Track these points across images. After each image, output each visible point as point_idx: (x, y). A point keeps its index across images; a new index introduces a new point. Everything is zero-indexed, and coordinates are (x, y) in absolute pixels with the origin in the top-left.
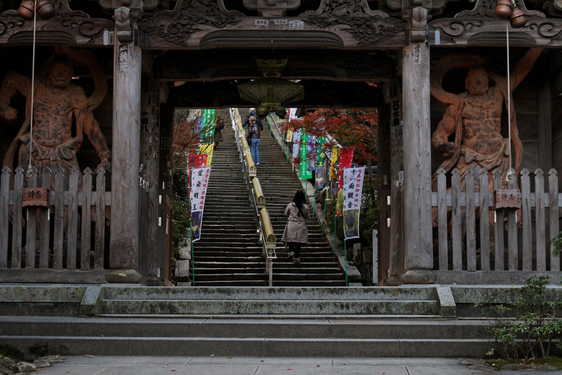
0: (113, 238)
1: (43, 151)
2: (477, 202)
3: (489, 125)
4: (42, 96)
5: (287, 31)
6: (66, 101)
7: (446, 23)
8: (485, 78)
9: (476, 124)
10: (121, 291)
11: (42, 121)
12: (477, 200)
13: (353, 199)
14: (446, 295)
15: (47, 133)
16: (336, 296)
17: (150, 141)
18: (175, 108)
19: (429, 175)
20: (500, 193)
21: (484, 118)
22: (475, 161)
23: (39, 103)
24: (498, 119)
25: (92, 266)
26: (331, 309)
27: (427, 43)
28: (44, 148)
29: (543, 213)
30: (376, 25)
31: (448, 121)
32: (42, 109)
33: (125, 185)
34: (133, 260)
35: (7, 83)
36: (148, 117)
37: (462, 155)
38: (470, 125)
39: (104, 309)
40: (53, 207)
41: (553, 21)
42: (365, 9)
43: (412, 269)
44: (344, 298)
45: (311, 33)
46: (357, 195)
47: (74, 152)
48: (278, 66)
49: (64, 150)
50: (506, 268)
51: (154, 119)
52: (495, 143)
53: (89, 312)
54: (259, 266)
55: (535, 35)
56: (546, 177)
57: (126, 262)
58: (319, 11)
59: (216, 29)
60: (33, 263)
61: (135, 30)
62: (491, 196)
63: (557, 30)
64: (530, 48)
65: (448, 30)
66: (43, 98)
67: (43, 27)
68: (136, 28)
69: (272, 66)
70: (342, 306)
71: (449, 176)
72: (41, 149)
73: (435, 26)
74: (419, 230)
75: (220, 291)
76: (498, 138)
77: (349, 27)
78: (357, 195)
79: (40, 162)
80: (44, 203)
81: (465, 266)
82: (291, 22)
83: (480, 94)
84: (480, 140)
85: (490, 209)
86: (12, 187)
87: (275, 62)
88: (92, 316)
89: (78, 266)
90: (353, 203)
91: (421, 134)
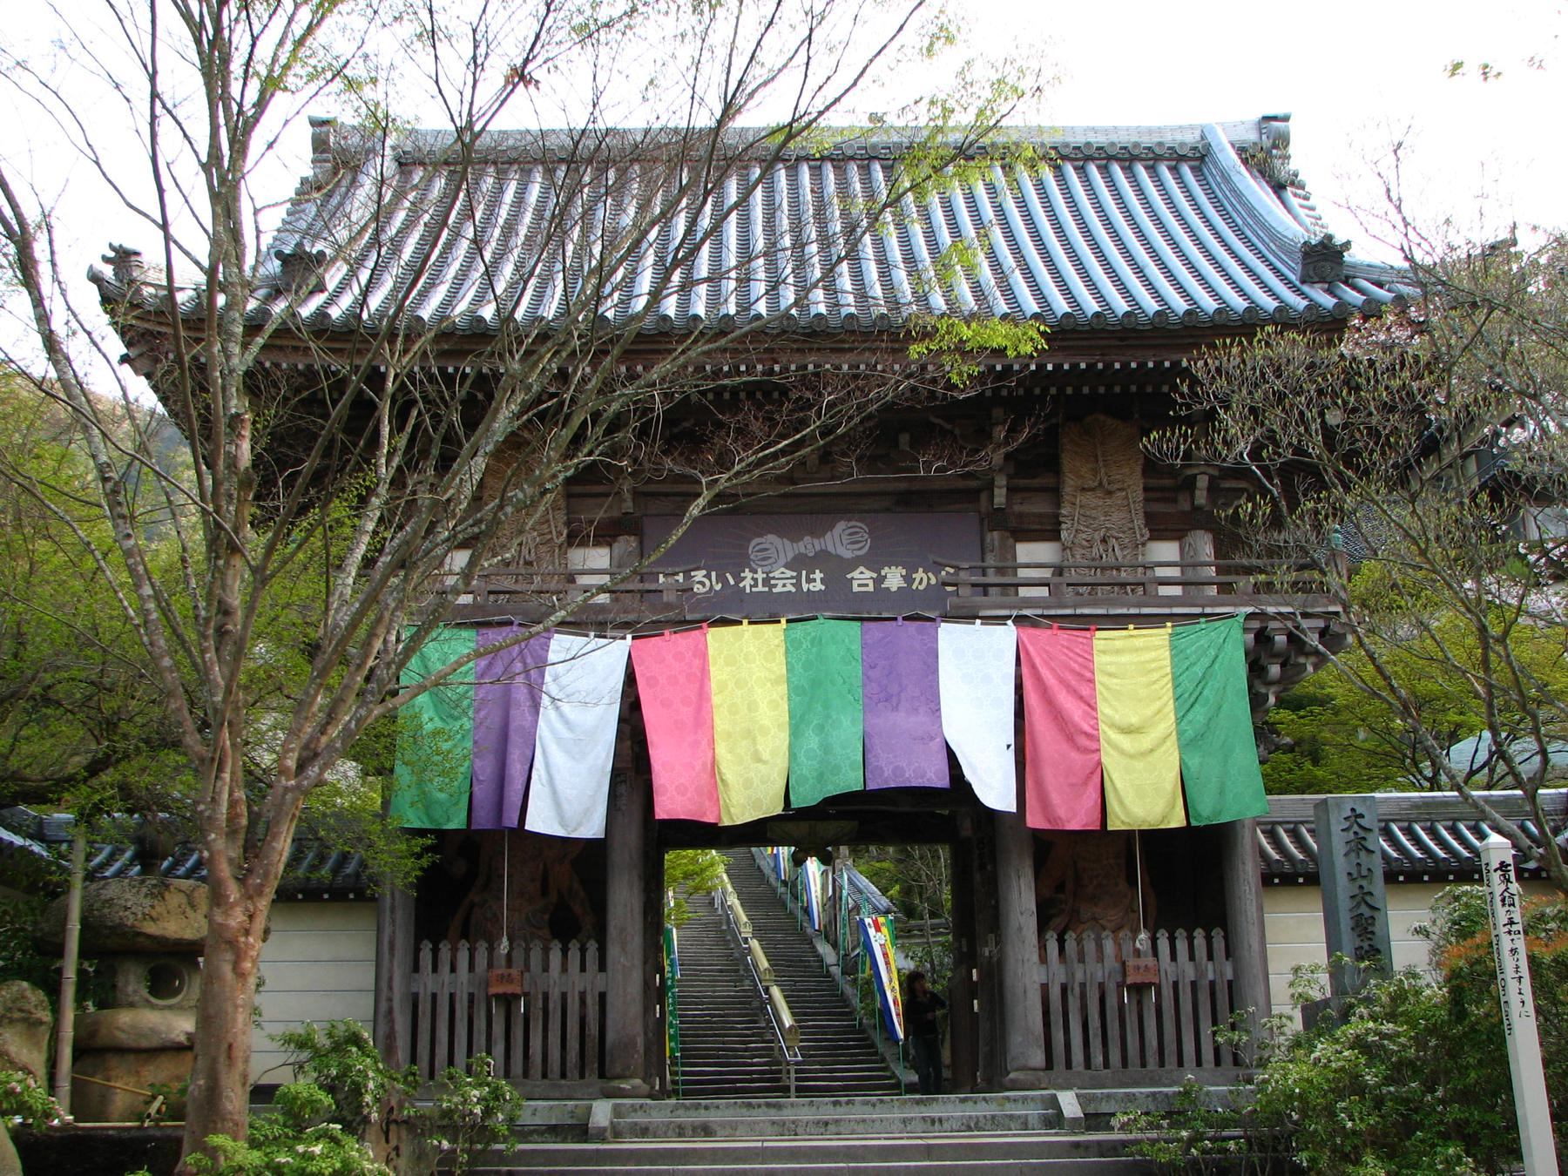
0: (611, 1036)
2: (1099, 977)
10: (634, 1109)
12: (1100, 974)
14: (1069, 1103)
16: (923, 1108)
20: (1131, 962)
25: (582, 1076)
26: (919, 1126)
29: (1188, 989)
39: (617, 1134)
44: (934, 1111)
47: (546, 917)
50: (1144, 1065)
53: (601, 1136)
54: (771, 1072)
56: (1191, 939)
62: (1117, 965)
70: (933, 1121)
74: (1026, 1014)
75: (768, 1105)
80: (518, 990)
81: (1088, 1063)
86: (471, 968)
88: (604, 1140)
89: (563, 1075)
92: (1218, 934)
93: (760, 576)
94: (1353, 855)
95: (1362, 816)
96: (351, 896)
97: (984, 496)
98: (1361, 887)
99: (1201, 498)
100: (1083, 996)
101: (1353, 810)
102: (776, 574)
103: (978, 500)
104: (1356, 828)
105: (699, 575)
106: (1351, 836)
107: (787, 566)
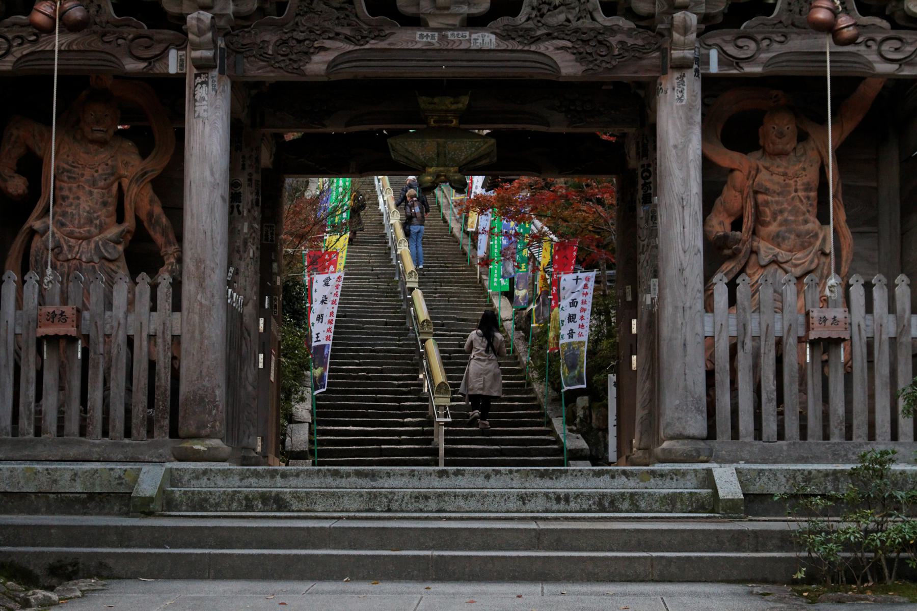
0: (184, 388)
1: (70, 246)
2: (778, 329)
3: (798, 204)
4: (68, 156)
5: (468, 51)
6: (107, 165)
7: (728, 38)
8: (792, 127)
9: (777, 203)
10: (197, 475)
11: (68, 198)
12: (778, 326)
13: (577, 325)
14: (727, 481)
15: (77, 217)
16: (549, 483)
17: (246, 230)
18: (286, 176)
19: (700, 286)
20: (815, 314)
21: (789, 193)
22: (775, 262)
23: (64, 168)
24: (813, 194)
25: (150, 433)
26: (540, 503)
27: (697, 71)
28: (72, 241)
29: (886, 348)
30: (613, 40)
31: (730, 197)
32: (69, 178)
33: (203, 301)
34: (218, 423)
35: (12, 135)
36: (241, 190)
37: (754, 252)
38: (767, 203)
39: (169, 504)
40: (86, 338)
41: (902, 34)
42: (596, 15)
43: (672, 438)
44: (561, 486)
45: (507, 54)
46: (582, 318)
47: (120, 248)
48: (454, 107)
49: (105, 244)
50: (826, 437)
51: (252, 193)
52: (808, 233)
53: (145, 508)
54: (423, 433)
55: (873, 57)
56: (891, 288)
57: (205, 426)
58: (521, 18)
59: (352, 47)
60: (54, 429)
61: (221, 49)
62: (801, 319)
63: (909, 49)
64: (864, 78)
65: (731, 50)
66: (71, 159)
67: (70, 44)
68: (223, 46)
69: (444, 107)
70: (558, 499)
71: (732, 286)
72: (67, 242)
73: (710, 42)
74: (684, 375)
75: (359, 474)
76: (813, 224)
77: (569, 44)
78: (582, 318)
79: (65, 264)
80: (72, 331)
81: (758, 433)
82: (474, 36)
83: (783, 154)
84: (783, 228)
85: (800, 340)
86: (19, 305)
87: (448, 100)
88: (150, 514)
89: (128, 434)
90: (577, 330)
91: (687, 218)
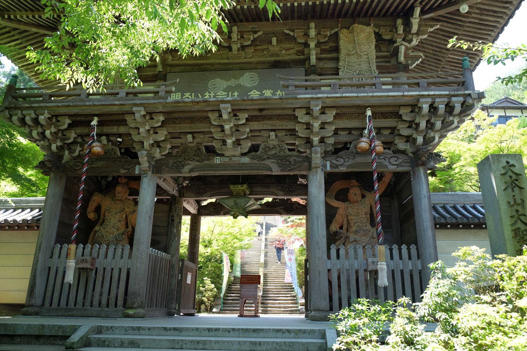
2: (356, 266)
3: (363, 220)
5: (239, 164)
7: (333, 158)
8: (359, 192)
9: (355, 219)
12: (356, 265)
19: (325, 249)
21: (359, 215)
22: (355, 241)
24: (368, 216)
27: (322, 169)
28: (108, 234)
30: (291, 159)
31: (339, 218)
37: (347, 237)
38: (351, 219)
41: (397, 155)
42: (285, 151)
43: (315, 310)
45: (253, 165)
48: (241, 188)
49: (119, 235)
52: (367, 230)
55: (387, 163)
56: (400, 250)
57: (135, 304)
58: (259, 152)
59: (198, 163)
60: (81, 304)
63: (400, 160)
65: (334, 162)
73: (327, 159)
76: (369, 227)
77: (276, 161)
80: (88, 266)
82: (241, 159)
83: (356, 202)
84: (358, 228)
85: (366, 271)
87: (240, 186)
91: (319, 223)
92: (413, 247)
93: (212, 95)
94: (510, 190)
95: (513, 166)
96: (461, 226)
97: (307, 62)
98: (517, 211)
99: (402, 58)
100: (411, 276)
101: (508, 162)
102: (219, 94)
103: (305, 64)
104: (510, 173)
105: (187, 95)
106: (508, 179)
107: (224, 91)
